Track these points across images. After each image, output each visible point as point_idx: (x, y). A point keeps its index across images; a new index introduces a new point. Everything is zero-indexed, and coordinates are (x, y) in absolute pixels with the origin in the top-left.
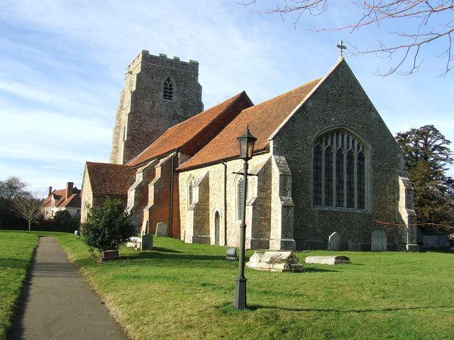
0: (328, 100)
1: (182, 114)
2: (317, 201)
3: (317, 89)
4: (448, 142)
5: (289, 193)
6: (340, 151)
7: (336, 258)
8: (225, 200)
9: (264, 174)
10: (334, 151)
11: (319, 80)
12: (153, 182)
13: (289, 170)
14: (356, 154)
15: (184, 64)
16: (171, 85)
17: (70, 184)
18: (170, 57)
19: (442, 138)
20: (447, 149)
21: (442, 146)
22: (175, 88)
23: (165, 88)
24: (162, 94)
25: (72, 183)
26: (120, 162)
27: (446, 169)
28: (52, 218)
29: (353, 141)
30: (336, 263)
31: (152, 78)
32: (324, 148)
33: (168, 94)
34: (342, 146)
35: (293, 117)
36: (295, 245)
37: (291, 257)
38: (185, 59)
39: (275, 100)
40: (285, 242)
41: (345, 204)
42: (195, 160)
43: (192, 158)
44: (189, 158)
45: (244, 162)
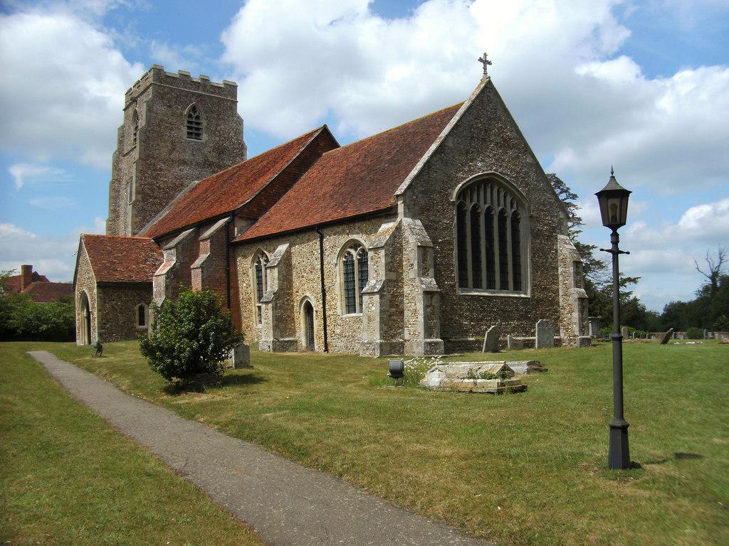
0: (472, 138)
1: (215, 160)
2: (463, 283)
3: (458, 121)
4: (574, 197)
5: (431, 272)
6: (489, 211)
7: (529, 364)
8: (323, 285)
9: (394, 248)
10: (497, 210)
11: (462, 104)
12: (198, 262)
13: (428, 239)
14: (509, 213)
15: (216, 88)
16: (197, 117)
17: (27, 269)
18: (196, 77)
19: (566, 191)
20: (574, 206)
21: (567, 201)
22: (204, 123)
23: (189, 122)
24: (185, 130)
25: (30, 267)
26: (130, 235)
27: (577, 232)
28: (631, 460)
29: (505, 197)
30: (528, 371)
31: (170, 107)
32: (469, 206)
33: (194, 131)
34: (492, 203)
35: (428, 162)
36: (442, 348)
37: (505, 368)
38: (217, 80)
39: (379, 137)
40: (430, 344)
41: (484, 283)
42: (263, 227)
43: (257, 224)
44: (252, 224)
45: (610, 231)
